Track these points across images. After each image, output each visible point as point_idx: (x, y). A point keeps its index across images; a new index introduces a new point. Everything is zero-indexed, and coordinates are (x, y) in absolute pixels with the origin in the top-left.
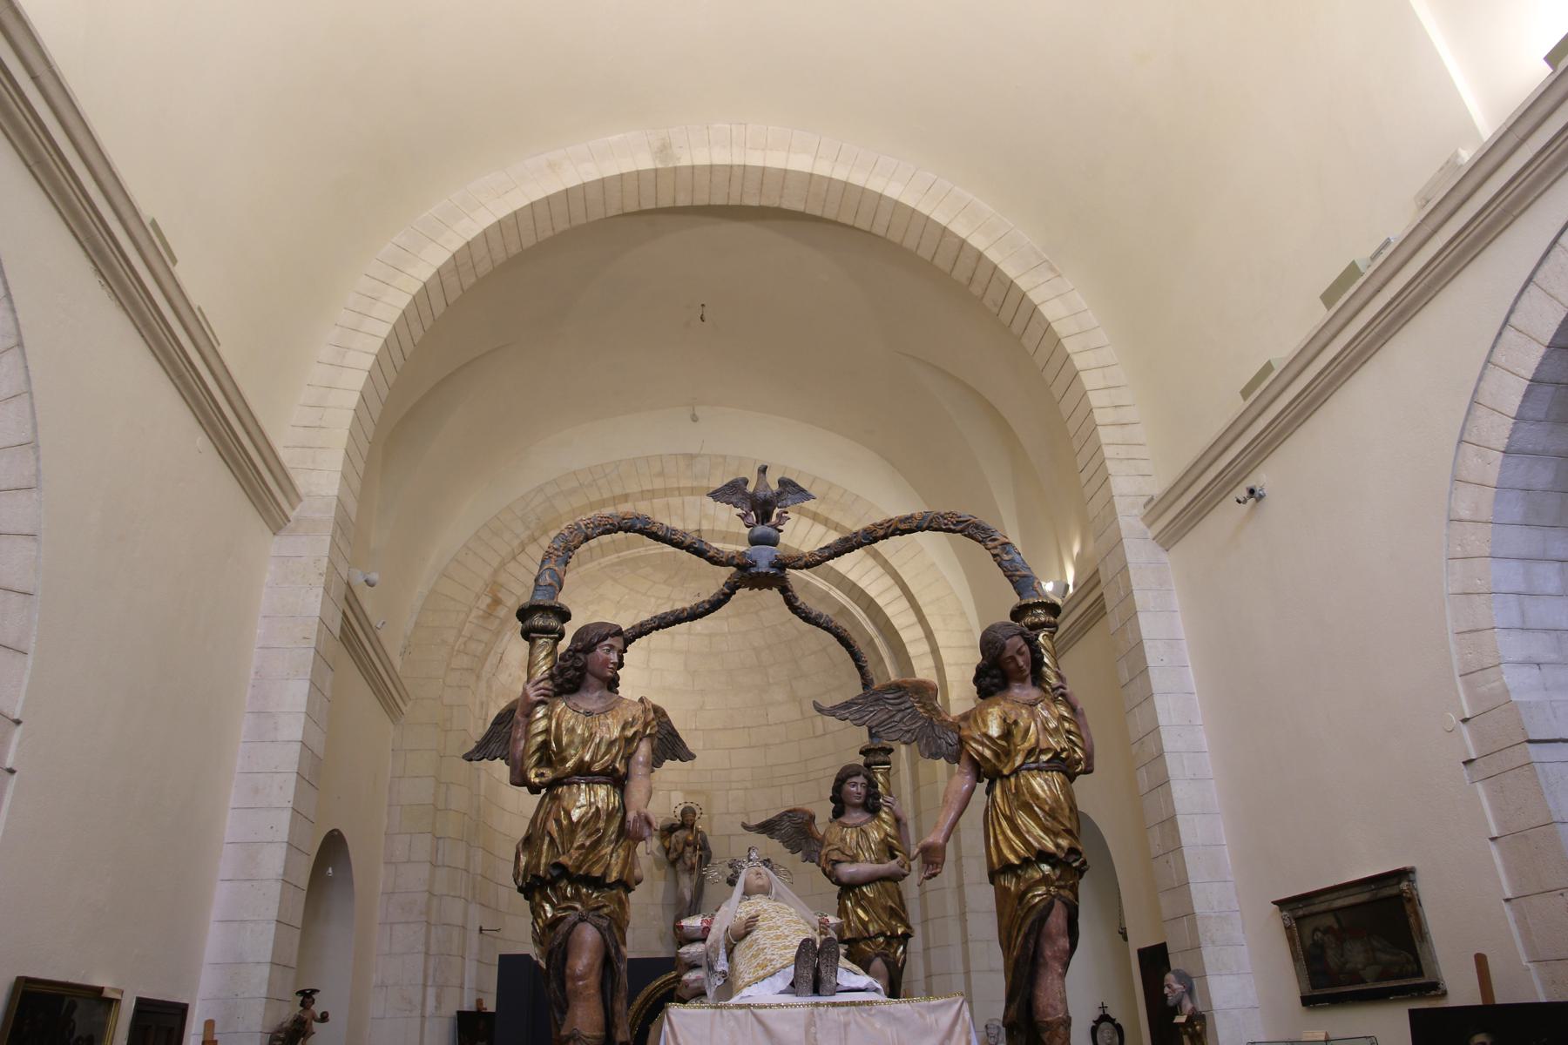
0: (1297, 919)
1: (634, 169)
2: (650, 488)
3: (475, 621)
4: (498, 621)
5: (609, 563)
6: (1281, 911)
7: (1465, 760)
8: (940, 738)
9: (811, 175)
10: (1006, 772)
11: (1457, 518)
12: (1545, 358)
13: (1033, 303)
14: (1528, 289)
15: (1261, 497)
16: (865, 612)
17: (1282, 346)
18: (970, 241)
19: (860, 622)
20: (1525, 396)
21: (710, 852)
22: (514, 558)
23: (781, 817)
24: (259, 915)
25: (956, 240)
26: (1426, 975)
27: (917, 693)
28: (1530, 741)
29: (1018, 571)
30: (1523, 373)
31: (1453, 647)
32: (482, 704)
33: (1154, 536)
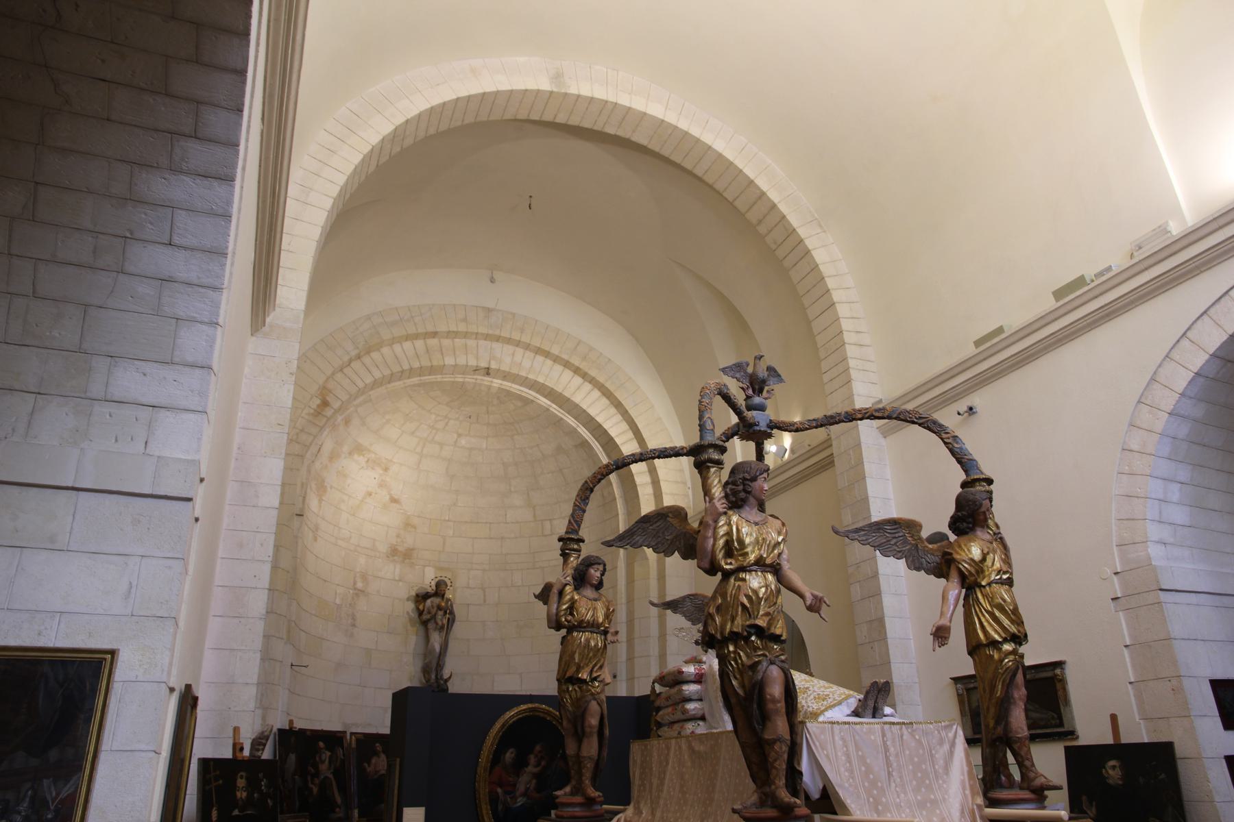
0: (968, 690)
1: (536, 87)
2: (455, 330)
3: (307, 417)
4: (325, 419)
5: (412, 383)
6: (956, 684)
7: (1114, 597)
8: (922, 558)
9: (663, 121)
10: (984, 583)
11: (1129, 449)
12: (1207, 361)
13: (807, 248)
14: (1202, 318)
15: (974, 413)
16: (602, 447)
17: (1015, 320)
18: (768, 194)
19: (597, 454)
20: (1190, 382)
21: (455, 616)
22: (341, 370)
23: (684, 598)
24: (246, 646)
25: (758, 191)
26: (1066, 725)
27: (907, 528)
28: (1161, 590)
29: (965, 455)
30: (1191, 367)
31: (1114, 527)
32: (303, 484)
33: (878, 426)
